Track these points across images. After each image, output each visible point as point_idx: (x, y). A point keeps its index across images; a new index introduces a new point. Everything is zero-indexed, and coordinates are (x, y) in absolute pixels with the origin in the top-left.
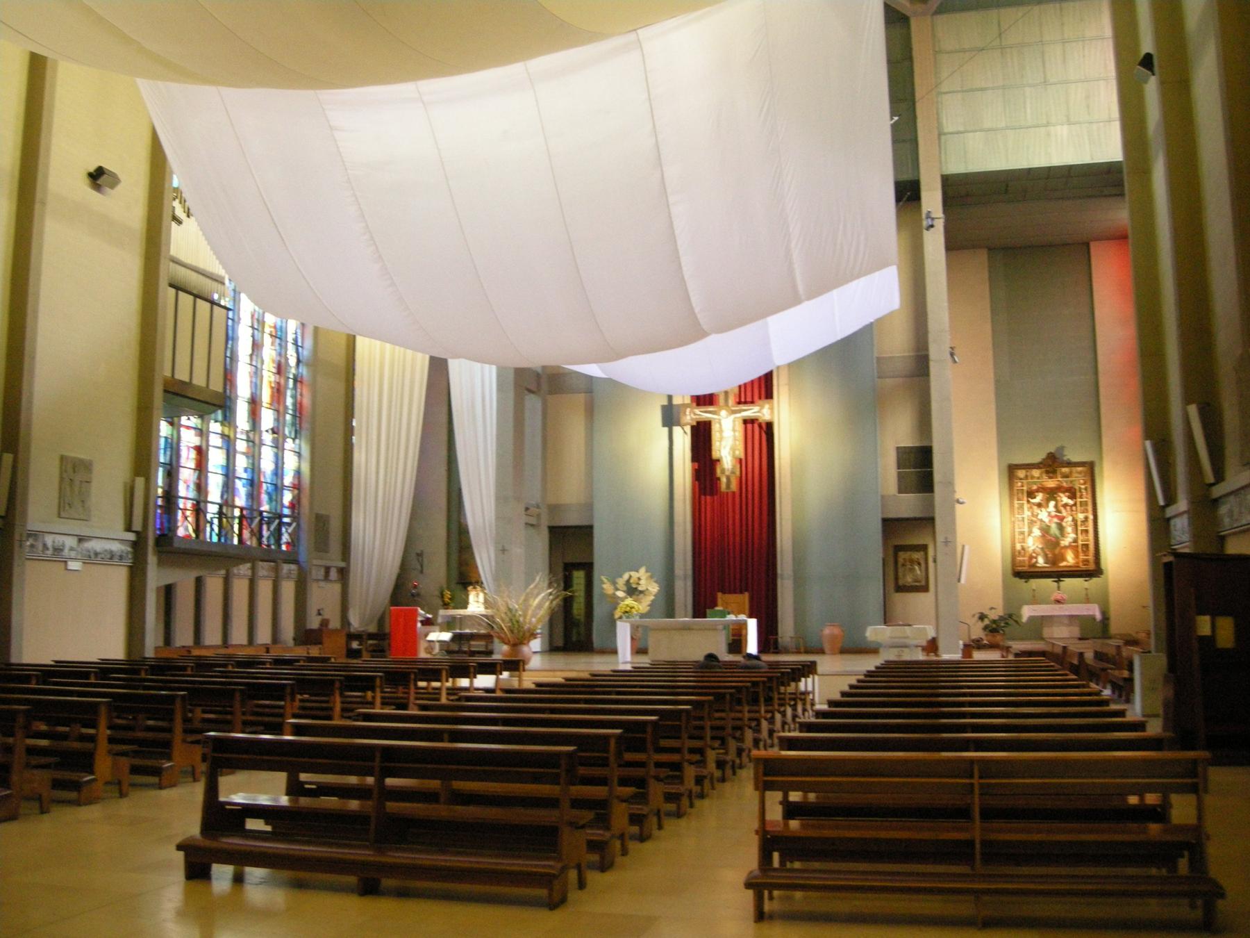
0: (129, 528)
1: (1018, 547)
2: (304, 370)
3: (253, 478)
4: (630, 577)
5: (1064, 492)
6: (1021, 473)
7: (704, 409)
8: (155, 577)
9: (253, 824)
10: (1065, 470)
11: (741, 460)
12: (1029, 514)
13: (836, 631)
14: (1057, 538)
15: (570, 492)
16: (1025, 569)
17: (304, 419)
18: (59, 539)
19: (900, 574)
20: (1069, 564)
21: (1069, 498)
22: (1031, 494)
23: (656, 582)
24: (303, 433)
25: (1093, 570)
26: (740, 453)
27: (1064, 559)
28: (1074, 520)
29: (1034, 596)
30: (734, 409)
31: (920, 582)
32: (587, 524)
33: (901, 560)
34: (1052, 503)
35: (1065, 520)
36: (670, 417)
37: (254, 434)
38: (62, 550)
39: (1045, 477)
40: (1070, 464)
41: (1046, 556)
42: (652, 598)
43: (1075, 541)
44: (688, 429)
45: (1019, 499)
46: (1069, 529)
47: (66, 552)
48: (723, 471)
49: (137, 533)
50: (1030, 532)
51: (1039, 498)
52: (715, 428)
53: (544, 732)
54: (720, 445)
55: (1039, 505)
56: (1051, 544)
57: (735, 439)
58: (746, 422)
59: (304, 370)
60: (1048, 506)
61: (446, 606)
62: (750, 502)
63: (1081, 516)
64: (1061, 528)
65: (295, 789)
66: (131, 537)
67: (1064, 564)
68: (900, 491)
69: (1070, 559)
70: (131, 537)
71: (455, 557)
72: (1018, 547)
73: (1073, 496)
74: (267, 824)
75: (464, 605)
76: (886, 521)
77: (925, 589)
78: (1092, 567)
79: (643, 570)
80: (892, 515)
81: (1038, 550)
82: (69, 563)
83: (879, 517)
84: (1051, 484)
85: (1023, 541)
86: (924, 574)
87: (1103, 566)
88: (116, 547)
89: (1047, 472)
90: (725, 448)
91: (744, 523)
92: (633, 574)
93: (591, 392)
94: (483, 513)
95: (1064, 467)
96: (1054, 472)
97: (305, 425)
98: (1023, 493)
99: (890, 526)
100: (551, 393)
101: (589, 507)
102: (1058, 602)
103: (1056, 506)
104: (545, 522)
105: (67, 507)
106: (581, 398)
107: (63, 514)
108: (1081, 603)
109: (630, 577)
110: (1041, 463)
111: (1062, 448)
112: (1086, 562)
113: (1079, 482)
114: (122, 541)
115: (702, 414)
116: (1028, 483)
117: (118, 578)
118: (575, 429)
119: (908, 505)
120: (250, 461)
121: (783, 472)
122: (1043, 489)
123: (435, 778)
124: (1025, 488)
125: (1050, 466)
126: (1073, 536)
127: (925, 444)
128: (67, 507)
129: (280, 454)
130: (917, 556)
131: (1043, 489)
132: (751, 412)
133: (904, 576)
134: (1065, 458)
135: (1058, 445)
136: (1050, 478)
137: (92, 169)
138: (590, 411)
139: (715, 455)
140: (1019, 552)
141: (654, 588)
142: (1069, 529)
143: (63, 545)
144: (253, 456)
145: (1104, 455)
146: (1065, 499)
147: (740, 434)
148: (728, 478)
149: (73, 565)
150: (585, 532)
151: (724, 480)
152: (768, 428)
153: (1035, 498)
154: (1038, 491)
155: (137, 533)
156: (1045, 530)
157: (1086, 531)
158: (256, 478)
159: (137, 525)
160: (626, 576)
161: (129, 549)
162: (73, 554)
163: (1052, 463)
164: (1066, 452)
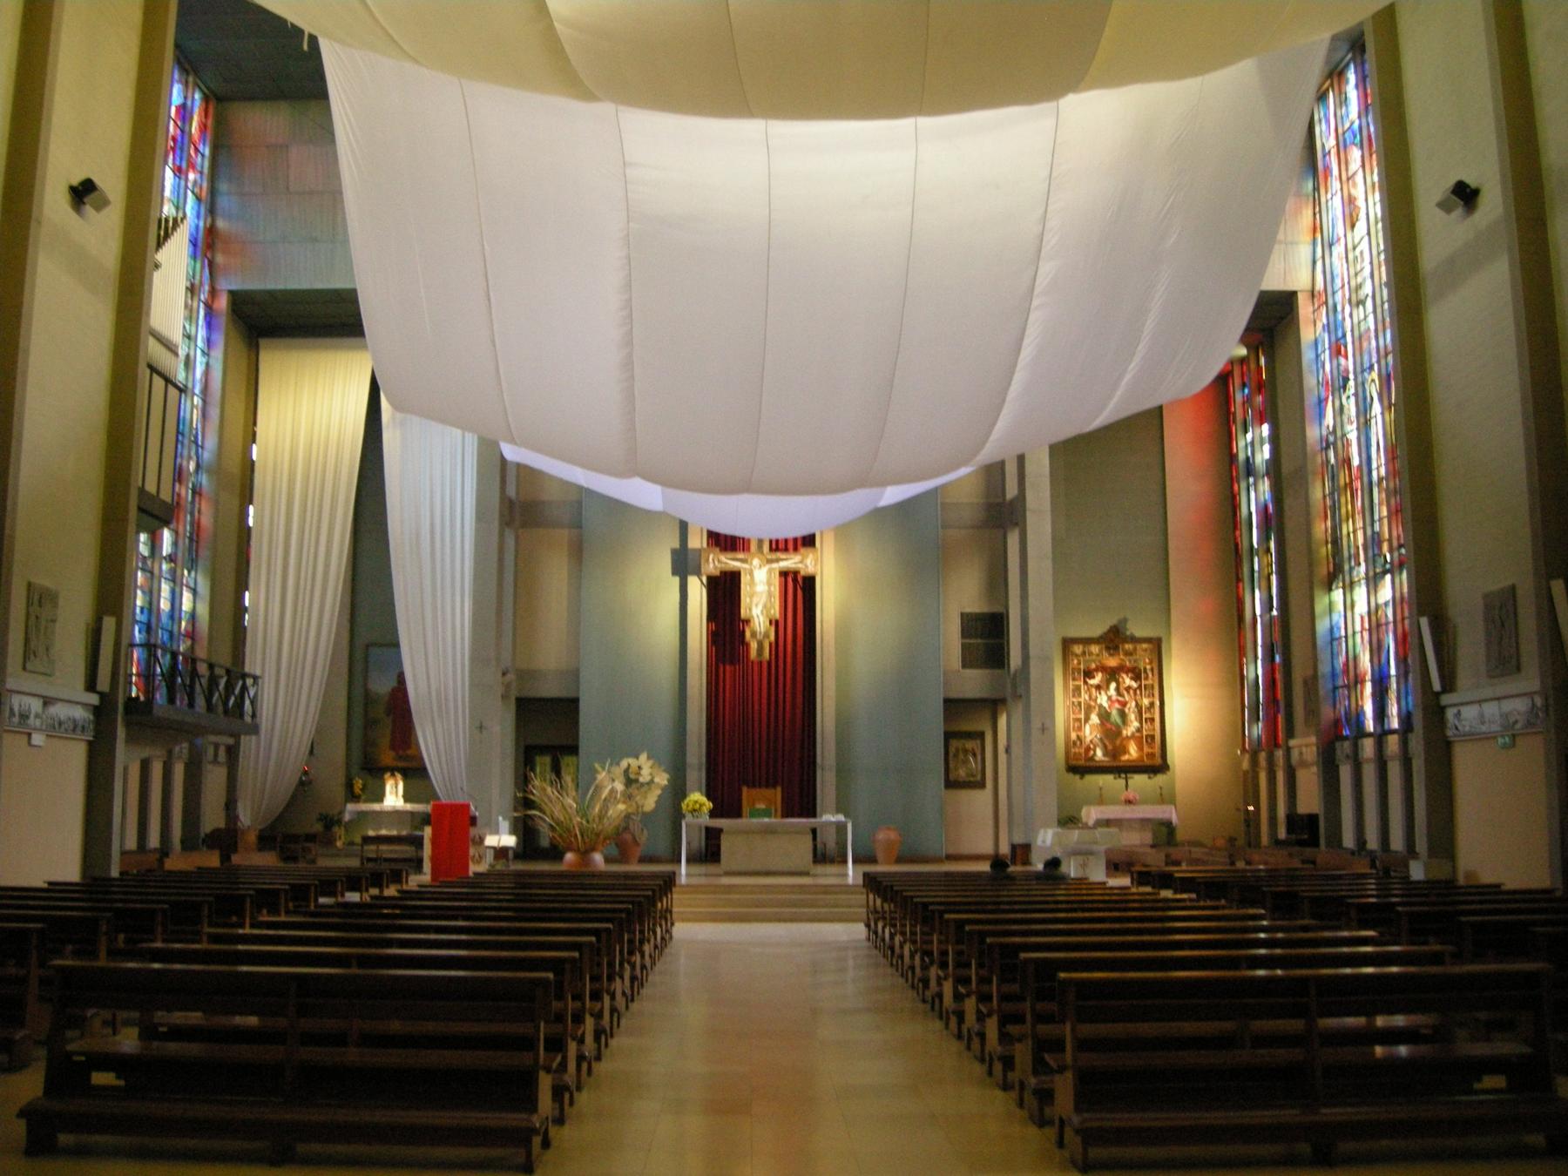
0: (91, 686)
1: (1073, 736)
2: (204, 479)
3: (149, 621)
4: (629, 765)
5: (1127, 673)
6: (1078, 649)
7: (730, 555)
8: (126, 758)
9: (101, 1078)
10: (1128, 646)
11: (777, 622)
12: (1087, 698)
13: (893, 835)
14: (1118, 727)
15: (550, 654)
16: (1082, 763)
17: (202, 543)
18: (27, 700)
19: (952, 765)
20: (1131, 758)
21: (1132, 679)
22: (1089, 674)
23: (665, 771)
24: (201, 562)
25: (1157, 766)
26: (776, 612)
27: (1125, 751)
28: (1138, 706)
29: (1101, 795)
30: (769, 557)
31: (973, 776)
32: (564, 694)
33: (952, 750)
34: (1113, 685)
35: (1128, 706)
36: (683, 564)
37: (153, 563)
38: (28, 717)
39: (1105, 654)
40: (1134, 640)
41: (1105, 747)
42: (659, 792)
43: (1139, 730)
44: (704, 579)
45: (1074, 679)
46: (1132, 717)
47: (31, 721)
48: (754, 634)
49: (102, 695)
50: (1087, 719)
51: (1098, 679)
52: (744, 579)
53: (1187, 978)
54: (751, 601)
55: (1098, 687)
56: (1111, 733)
57: (770, 595)
58: (784, 574)
59: (204, 479)
60: (1108, 688)
61: (355, 798)
62: (781, 678)
63: (1146, 702)
64: (1123, 715)
65: (149, 1032)
66: (94, 699)
67: (1126, 757)
68: (964, 666)
69: (1133, 752)
70: (94, 699)
71: (357, 735)
72: (1073, 736)
73: (1137, 678)
74: (118, 1077)
75: (380, 797)
76: (949, 703)
77: (981, 785)
78: (1158, 761)
79: (643, 757)
80: (954, 695)
81: (1096, 740)
82: (34, 736)
83: (942, 696)
84: (1112, 662)
85: (1080, 729)
86: (980, 768)
87: (1169, 762)
88: (80, 713)
89: (1108, 648)
90: (757, 605)
91: (773, 698)
92: (632, 761)
93: (581, 527)
94: (428, 678)
95: (1127, 642)
96: (1116, 648)
97: (205, 553)
98: (1079, 673)
99: (953, 706)
100: (524, 525)
101: (575, 675)
102: (1129, 802)
103: (1117, 689)
104: (514, 694)
105: (32, 657)
106: (564, 534)
107: (29, 666)
108: (1153, 803)
109: (629, 765)
110: (1101, 637)
111: (1125, 621)
112: (1151, 755)
113: (1145, 662)
114: (85, 705)
115: (729, 562)
116: (1085, 661)
117: (76, 755)
118: (555, 575)
119: (974, 683)
120: (148, 598)
121: (825, 638)
122: (1103, 669)
123: (195, 1010)
124: (1082, 667)
125: (1112, 641)
126: (1136, 724)
127: (998, 609)
128: (32, 657)
129: (178, 590)
130: (970, 745)
131: (1103, 669)
132: (790, 562)
133: (956, 769)
134: (1128, 633)
135: (1121, 616)
136: (1111, 655)
137: (75, 181)
138: (578, 552)
139: (744, 614)
140: (1074, 743)
141: (662, 779)
142: (1132, 717)
143: (29, 711)
144: (151, 592)
145: (1173, 630)
146: (1128, 681)
147: (776, 590)
148: (760, 645)
149: (38, 739)
150: (568, 708)
151: (754, 646)
152: (808, 584)
153: (1094, 677)
154: (1097, 670)
155: (102, 695)
156: (1104, 716)
157: (1152, 720)
158: (154, 620)
159: (103, 683)
160: (624, 764)
161: (91, 717)
162: (38, 722)
163: (1114, 638)
164: (1129, 626)
